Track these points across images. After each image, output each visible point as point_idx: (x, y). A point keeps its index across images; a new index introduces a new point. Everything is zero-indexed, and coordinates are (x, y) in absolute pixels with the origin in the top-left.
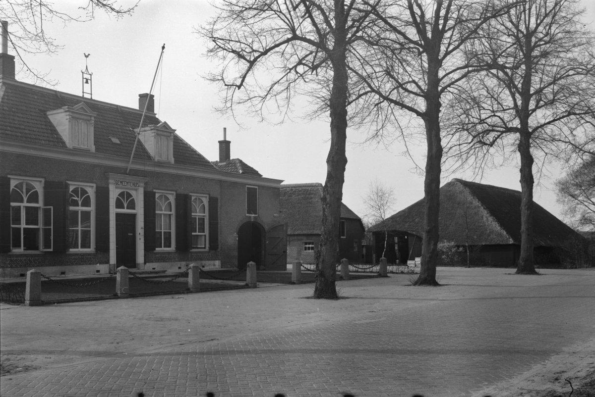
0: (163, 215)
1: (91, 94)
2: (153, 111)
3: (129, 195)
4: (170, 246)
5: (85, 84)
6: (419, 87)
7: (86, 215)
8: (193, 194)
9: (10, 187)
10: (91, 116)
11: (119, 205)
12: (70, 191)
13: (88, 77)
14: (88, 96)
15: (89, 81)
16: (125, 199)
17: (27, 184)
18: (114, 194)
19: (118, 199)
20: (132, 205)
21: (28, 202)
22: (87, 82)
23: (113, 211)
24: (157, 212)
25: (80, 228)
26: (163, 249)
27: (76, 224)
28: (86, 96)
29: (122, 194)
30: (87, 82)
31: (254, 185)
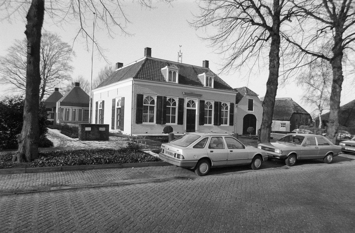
0: (149, 107)
3: (193, 102)
5: (179, 57)
6: (334, 8)
7: (174, 109)
8: (206, 100)
9: (143, 99)
11: (188, 105)
13: (181, 54)
14: (181, 62)
15: (181, 56)
17: (192, 101)
18: (186, 101)
20: (194, 105)
21: (172, 106)
22: (180, 57)
23: (186, 107)
24: (222, 110)
26: (148, 123)
27: (147, 112)
28: (179, 62)
29: (189, 101)
30: (180, 57)
31: (192, 87)
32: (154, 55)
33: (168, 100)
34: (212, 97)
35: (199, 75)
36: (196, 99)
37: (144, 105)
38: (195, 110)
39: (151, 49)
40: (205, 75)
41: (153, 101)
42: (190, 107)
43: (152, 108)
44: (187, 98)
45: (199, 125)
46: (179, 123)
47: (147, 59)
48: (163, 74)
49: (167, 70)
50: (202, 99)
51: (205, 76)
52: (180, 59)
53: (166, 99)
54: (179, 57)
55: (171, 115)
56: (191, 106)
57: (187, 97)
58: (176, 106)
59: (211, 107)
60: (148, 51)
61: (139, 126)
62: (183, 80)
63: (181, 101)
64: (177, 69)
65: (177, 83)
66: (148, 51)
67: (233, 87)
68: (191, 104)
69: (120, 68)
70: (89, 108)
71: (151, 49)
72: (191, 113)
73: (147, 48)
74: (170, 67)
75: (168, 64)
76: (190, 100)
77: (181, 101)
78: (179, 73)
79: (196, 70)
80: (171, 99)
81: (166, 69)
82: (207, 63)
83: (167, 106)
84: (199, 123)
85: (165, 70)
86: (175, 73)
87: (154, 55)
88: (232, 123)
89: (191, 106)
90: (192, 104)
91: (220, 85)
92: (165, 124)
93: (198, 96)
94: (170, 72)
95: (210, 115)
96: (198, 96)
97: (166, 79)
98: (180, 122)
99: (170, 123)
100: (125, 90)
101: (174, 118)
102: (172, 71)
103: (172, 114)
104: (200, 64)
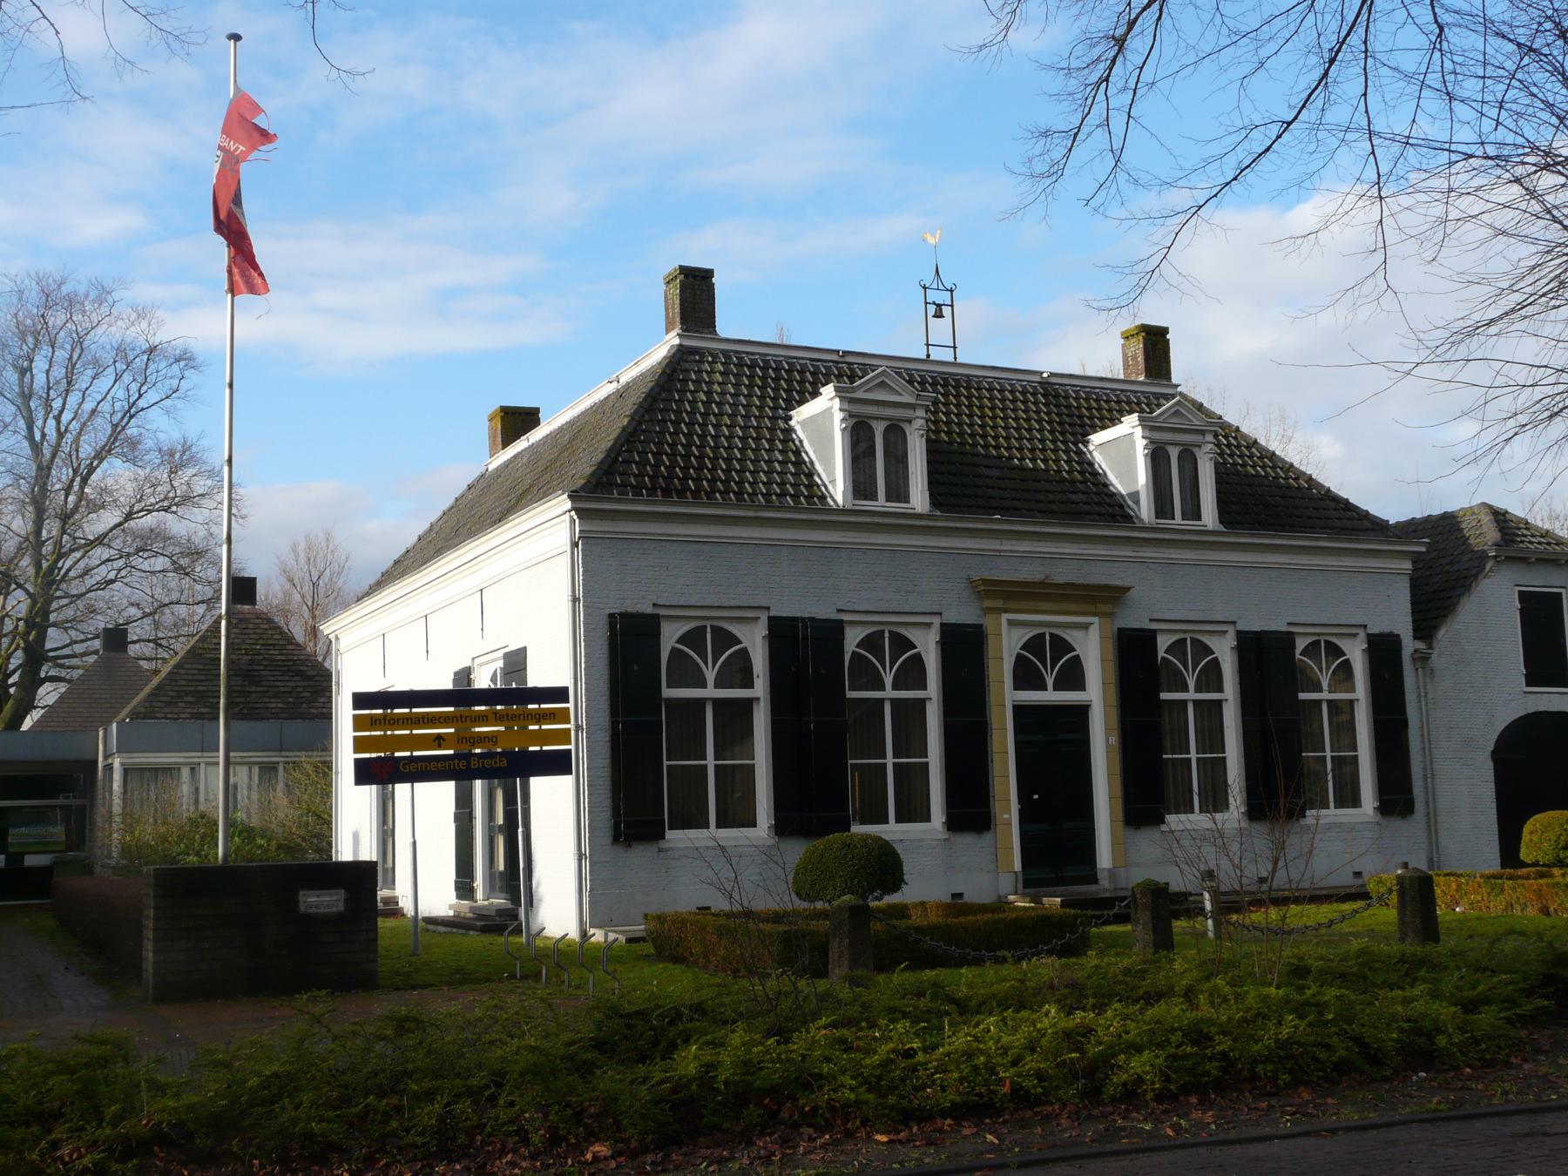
1: (955, 348)
2: (1169, 379)
3: (1062, 646)
4: (1355, 802)
7: (1342, 711)
10: (1203, 433)
11: (1026, 676)
12: (1298, 651)
13: (944, 297)
14: (947, 355)
15: (946, 311)
16: (1047, 657)
18: (1007, 642)
19: (1020, 660)
20: (1073, 676)
21: (895, 687)
22: (939, 315)
23: (1005, 697)
25: (1328, 754)
26: (1198, 820)
28: (936, 354)
29: (1035, 645)
30: (939, 315)
32: (735, 321)
34: (1217, 599)
35: (1097, 438)
36: (1086, 627)
37: (668, 693)
38: (1082, 711)
39: (1165, 331)
40: (1139, 432)
41: (917, 663)
42: (1045, 688)
43: (735, 716)
44: (1005, 617)
45: (616, 839)
46: (956, 823)
47: (679, 361)
48: (810, 451)
49: (838, 416)
50: (1135, 619)
51: (1140, 444)
56: (1050, 682)
57: (1006, 611)
58: (1220, 689)
59: (1211, 679)
60: (694, 293)
61: (639, 855)
62: (967, 483)
63: (964, 646)
64: (912, 407)
65: (919, 510)
66: (694, 293)
67: (1392, 508)
69: (521, 445)
70: (359, 745)
71: (1165, 331)
72: (1053, 741)
73: (681, 267)
74: (860, 395)
75: (844, 370)
76: (1182, 636)
77: (964, 646)
78: (1221, 454)
79: (1076, 407)
81: (828, 412)
82: (1154, 343)
83: (1164, 696)
84: (616, 826)
85: (820, 423)
86: (896, 433)
87: (735, 321)
88: (1396, 799)
89: (1050, 682)
90: (1328, 668)
91: (1270, 501)
93: (1101, 598)
94: (859, 434)
95: (1212, 737)
96: (1101, 598)
97: (833, 482)
98: (970, 813)
100: (516, 605)
101: (911, 780)
102: (874, 424)
104: (1099, 355)
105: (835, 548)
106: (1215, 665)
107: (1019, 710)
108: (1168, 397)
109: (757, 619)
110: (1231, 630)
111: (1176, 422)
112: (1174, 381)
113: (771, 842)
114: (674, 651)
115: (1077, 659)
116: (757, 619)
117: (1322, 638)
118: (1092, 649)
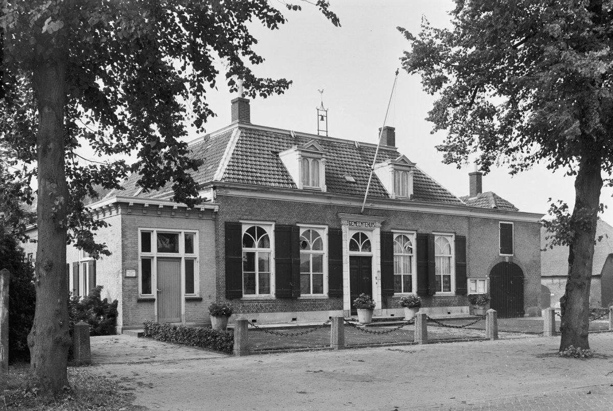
2: (394, 146)
3: (364, 237)
10: (322, 154)
11: (353, 246)
13: (324, 113)
14: (324, 134)
15: (325, 118)
16: (360, 240)
18: (347, 235)
19: (352, 241)
20: (368, 246)
22: (322, 119)
23: (347, 253)
28: (322, 134)
29: (356, 236)
31: (508, 221)
33: (303, 235)
38: (369, 259)
52: (323, 125)
53: (299, 233)
54: (320, 121)
55: (311, 273)
56: (360, 248)
68: (309, 239)
75: (296, 140)
80: (255, 227)
82: (389, 133)
89: (360, 248)
90: (258, 239)
92: (393, 295)
99: (441, 291)
103: (309, 275)
104: (374, 138)
105: (453, 216)
106: (320, 240)
107: (351, 257)
108: (398, 156)
109: (324, 228)
110: (274, 224)
111: (312, 150)
112: (396, 146)
113: (274, 299)
114: (245, 234)
115: (320, 239)
116: (271, 225)
117: (256, 226)
118: (375, 238)
